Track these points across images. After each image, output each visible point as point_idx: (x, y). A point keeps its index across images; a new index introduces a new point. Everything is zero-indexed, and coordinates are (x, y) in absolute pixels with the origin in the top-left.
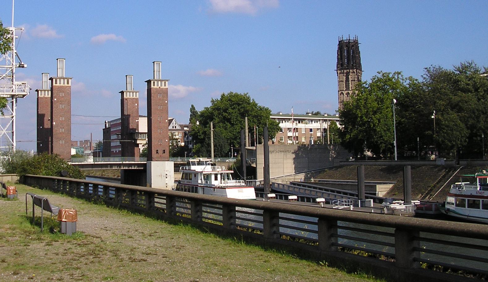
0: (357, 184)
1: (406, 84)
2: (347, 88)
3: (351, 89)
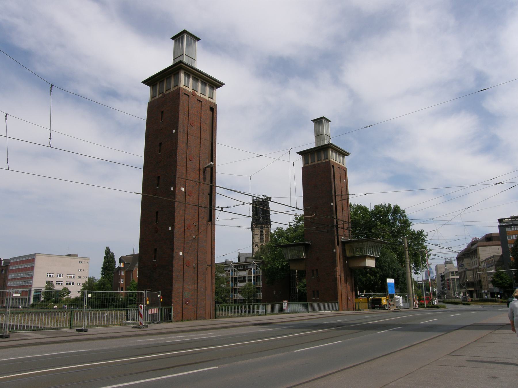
0: (65, 326)
1: (75, 298)
2: (262, 240)
3: (265, 242)
